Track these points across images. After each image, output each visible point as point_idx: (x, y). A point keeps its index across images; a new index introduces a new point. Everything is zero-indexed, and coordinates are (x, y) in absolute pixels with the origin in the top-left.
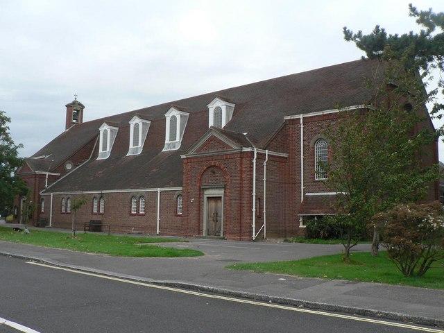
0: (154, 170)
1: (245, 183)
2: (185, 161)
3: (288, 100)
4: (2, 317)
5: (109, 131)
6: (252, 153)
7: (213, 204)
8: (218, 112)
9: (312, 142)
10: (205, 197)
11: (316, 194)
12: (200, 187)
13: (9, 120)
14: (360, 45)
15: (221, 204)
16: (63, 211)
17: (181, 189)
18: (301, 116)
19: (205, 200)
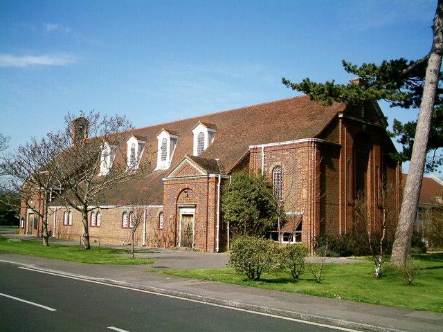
0: (145, 188)
1: (210, 204)
2: (165, 183)
3: (304, 114)
4: (440, 186)
5: (206, 135)
6: (217, 178)
7: (187, 219)
8: (201, 140)
9: (271, 169)
10: (181, 214)
11: (13, 298)
12: (176, 206)
13: (384, 62)
14: (96, 139)
15: (193, 220)
16: (66, 223)
17: (162, 206)
18: (262, 146)
19: (181, 216)
